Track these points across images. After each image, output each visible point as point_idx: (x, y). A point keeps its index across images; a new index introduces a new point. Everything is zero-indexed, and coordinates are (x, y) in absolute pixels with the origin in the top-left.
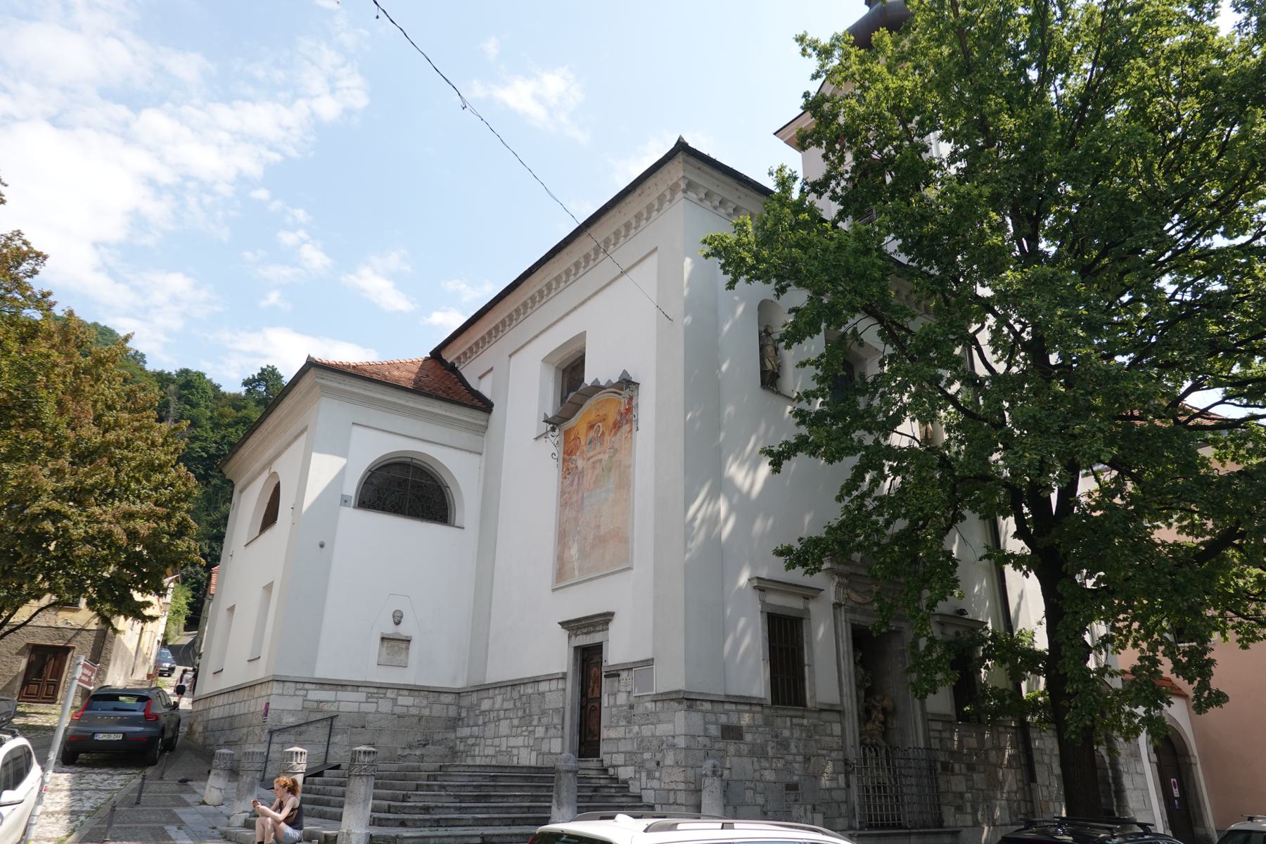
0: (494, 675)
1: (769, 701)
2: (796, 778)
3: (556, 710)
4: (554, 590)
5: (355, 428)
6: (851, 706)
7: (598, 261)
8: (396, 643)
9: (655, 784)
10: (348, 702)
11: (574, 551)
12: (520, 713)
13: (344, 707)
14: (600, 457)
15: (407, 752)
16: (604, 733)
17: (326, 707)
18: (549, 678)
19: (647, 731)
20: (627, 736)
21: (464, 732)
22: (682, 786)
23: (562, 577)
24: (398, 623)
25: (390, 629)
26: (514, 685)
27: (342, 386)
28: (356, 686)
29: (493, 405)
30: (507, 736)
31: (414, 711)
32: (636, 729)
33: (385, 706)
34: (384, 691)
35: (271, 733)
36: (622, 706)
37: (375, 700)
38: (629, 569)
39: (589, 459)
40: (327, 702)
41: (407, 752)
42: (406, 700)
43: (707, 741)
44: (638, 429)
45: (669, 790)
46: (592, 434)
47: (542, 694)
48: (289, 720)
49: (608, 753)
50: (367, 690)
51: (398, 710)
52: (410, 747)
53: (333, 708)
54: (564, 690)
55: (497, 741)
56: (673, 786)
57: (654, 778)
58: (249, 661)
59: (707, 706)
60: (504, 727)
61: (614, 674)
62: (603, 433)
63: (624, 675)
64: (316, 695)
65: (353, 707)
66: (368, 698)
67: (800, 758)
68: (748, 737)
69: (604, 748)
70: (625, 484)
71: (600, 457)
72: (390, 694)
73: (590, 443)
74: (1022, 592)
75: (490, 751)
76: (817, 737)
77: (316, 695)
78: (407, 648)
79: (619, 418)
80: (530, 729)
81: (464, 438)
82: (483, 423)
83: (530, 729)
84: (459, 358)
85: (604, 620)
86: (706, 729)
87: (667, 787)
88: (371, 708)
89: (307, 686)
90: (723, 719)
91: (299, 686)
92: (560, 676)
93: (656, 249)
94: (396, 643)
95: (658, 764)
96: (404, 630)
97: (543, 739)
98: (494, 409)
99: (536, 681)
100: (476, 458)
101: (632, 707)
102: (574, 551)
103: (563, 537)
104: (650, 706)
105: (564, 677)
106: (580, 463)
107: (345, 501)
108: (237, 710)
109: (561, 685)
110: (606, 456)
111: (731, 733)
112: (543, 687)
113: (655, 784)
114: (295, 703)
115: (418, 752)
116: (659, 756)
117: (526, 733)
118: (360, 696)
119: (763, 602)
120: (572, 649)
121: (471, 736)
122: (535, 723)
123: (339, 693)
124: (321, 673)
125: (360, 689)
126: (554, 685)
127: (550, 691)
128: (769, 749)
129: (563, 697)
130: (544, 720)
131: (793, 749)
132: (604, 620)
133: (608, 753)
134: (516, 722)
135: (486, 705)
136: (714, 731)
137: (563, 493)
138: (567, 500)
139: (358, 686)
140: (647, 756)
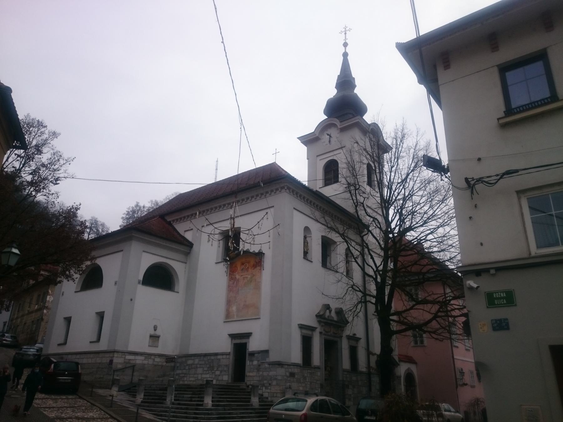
0: (193, 350)
1: (302, 365)
2: (308, 389)
3: (226, 366)
4: (224, 322)
5: (144, 254)
6: (323, 367)
7: (247, 202)
8: (155, 338)
9: (269, 391)
10: (139, 360)
11: (234, 308)
12: (208, 366)
13: (138, 362)
14: (247, 276)
15: (158, 379)
16: (247, 374)
17: (132, 362)
18: (222, 354)
19: (265, 374)
20: (257, 375)
21: (179, 372)
22: (279, 391)
23: (228, 318)
24: (155, 330)
25: (153, 332)
26: (206, 355)
27: (141, 237)
28: (141, 354)
29: (193, 245)
30: (201, 374)
31: (160, 364)
32: (261, 373)
33: (151, 362)
34: (150, 356)
35: (114, 371)
36: (255, 365)
37: (147, 359)
38: (259, 318)
39: (241, 276)
40: (132, 360)
41: (158, 379)
42: (158, 359)
43: (285, 377)
44: (263, 270)
45: (274, 393)
46: (243, 267)
47: (219, 359)
48: (120, 366)
49: (249, 381)
50: (145, 355)
51: (155, 363)
52: (159, 377)
53: (134, 362)
54: (229, 358)
55: (195, 376)
56: (276, 391)
57: (268, 389)
58: (91, 342)
59: (286, 366)
60: (200, 371)
61: (252, 354)
62: (248, 267)
63: (256, 355)
64: (129, 357)
65: (140, 362)
66: (145, 358)
67: (309, 383)
68: (296, 376)
69: (247, 379)
70: (258, 287)
71: (247, 276)
72: (153, 357)
73: (242, 270)
74: (217, 161)
75: (191, 379)
76: (314, 376)
77: (129, 357)
78: (158, 340)
79: (255, 264)
80: (213, 371)
81: (180, 257)
82: (189, 251)
83: (213, 371)
84: (173, 221)
85: (248, 335)
86: (286, 374)
87: (273, 391)
88: (146, 362)
89: (126, 354)
90: (290, 370)
91: (123, 354)
92: (228, 353)
93: (273, 206)
94: (155, 338)
95: (270, 384)
96: (158, 333)
97: (219, 375)
98: (194, 246)
99: (216, 354)
100: (183, 265)
101: (259, 366)
102: (234, 308)
103: (229, 303)
104: (267, 365)
105: (229, 354)
106: (237, 277)
107: (139, 283)
108: (80, 361)
109: (228, 357)
110: (249, 276)
111: (292, 375)
112: (219, 357)
113: (269, 391)
114: (121, 360)
115: (161, 379)
116: (270, 382)
117: (211, 373)
118: (142, 358)
119: (301, 332)
120: (233, 344)
121: (182, 373)
122: (215, 369)
123: (136, 356)
124: (131, 348)
125: (143, 355)
126: (224, 357)
127: (223, 358)
128: (301, 380)
129: (229, 361)
130: (220, 369)
131: (307, 380)
132: (248, 335)
133: (249, 381)
134: (206, 369)
135: (190, 362)
136: (288, 374)
137: (229, 286)
138: (230, 289)
139: (142, 354)
140: (265, 382)
